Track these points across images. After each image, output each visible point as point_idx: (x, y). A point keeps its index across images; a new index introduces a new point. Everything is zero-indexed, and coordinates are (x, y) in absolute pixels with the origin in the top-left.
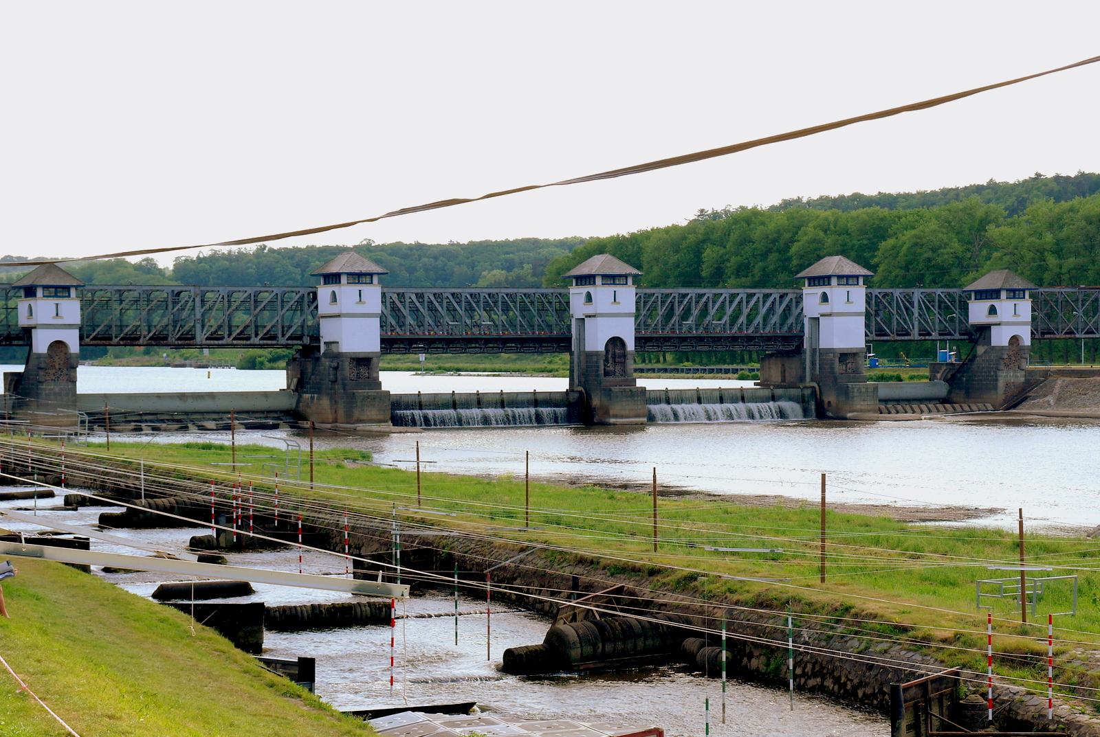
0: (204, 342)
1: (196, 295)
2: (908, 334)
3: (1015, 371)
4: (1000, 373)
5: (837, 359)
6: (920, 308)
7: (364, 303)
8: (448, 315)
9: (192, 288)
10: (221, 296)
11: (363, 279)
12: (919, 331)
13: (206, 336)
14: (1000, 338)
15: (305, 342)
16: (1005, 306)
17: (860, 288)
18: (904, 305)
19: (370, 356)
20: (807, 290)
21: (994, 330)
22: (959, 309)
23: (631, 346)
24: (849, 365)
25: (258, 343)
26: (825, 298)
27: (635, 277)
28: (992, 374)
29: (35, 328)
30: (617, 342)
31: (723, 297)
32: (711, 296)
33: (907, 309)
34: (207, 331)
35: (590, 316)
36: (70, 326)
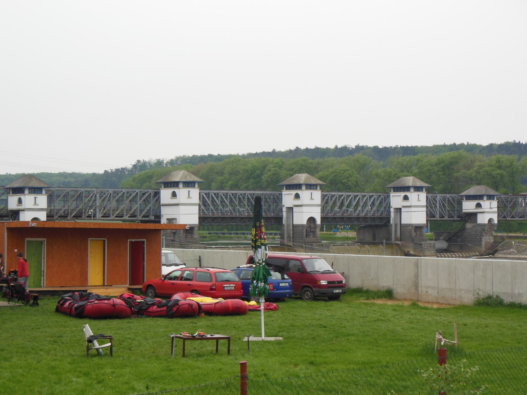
0: (101, 218)
1: (97, 193)
2: (434, 217)
3: (489, 237)
4: (483, 237)
5: (413, 230)
6: (440, 204)
7: (191, 198)
8: (221, 205)
9: (95, 189)
10: (109, 194)
11: (190, 185)
12: (439, 215)
13: (102, 215)
14: (482, 219)
15: (151, 219)
16: (486, 204)
17: (196, 189)
18: (433, 202)
19: (193, 226)
20: (285, 192)
21: (479, 216)
22: (457, 204)
23: (319, 222)
24: (418, 232)
25: (127, 219)
26: (174, 195)
27: (321, 186)
28: (478, 237)
29: (23, 210)
30: (312, 220)
31: (351, 197)
32: (345, 196)
33: (434, 204)
34: (102, 213)
35: (297, 206)
36: (42, 210)
